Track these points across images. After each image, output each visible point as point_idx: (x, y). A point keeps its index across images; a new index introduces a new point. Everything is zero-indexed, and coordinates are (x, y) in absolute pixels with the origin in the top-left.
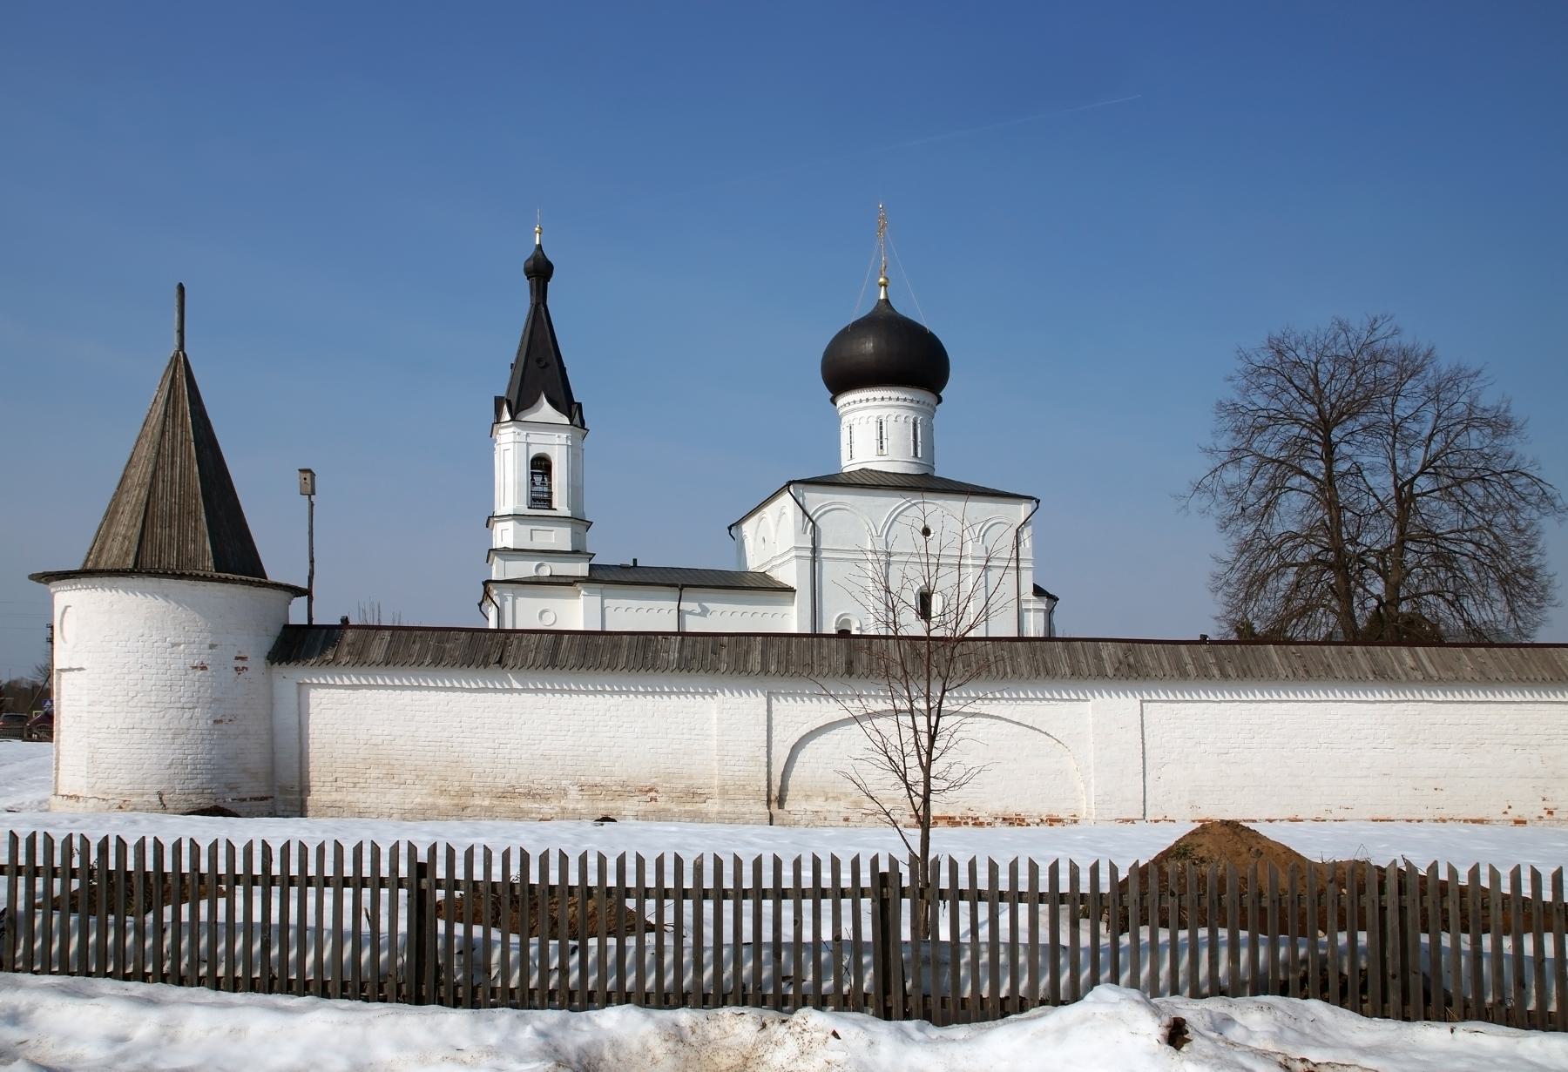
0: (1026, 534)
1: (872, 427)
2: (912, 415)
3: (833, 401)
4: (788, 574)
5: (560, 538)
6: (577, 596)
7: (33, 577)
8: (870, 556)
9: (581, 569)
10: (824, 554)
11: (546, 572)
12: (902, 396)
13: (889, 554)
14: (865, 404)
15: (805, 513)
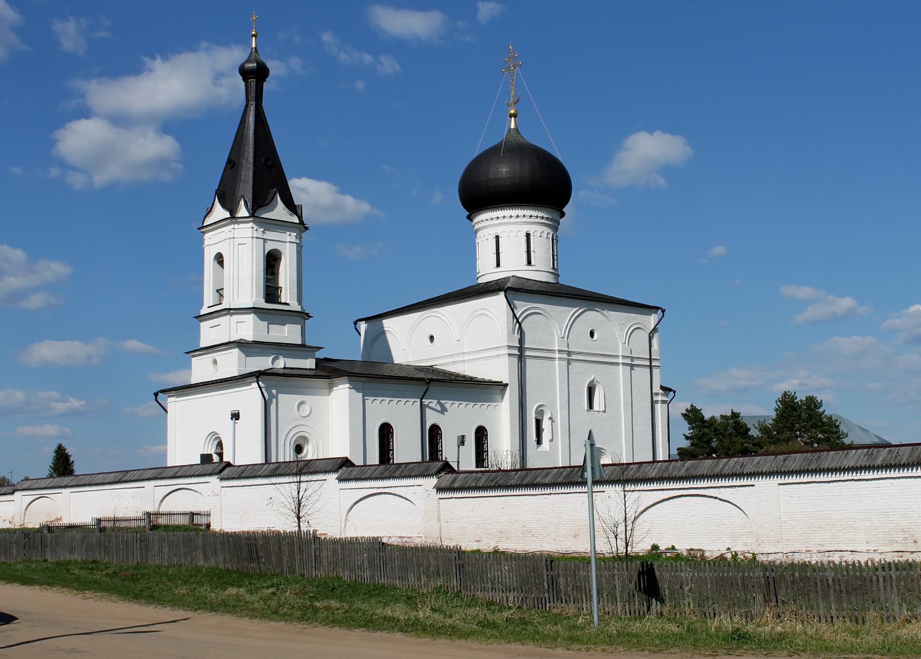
0: (655, 341)
1: (509, 240)
2: (547, 230)
3: (470, 218)
4: (498, 368)
5: (289, 333)
6: (331, 388)
7: (590, 432)
8: (557, 355)
9: (309, 363)
10: (527, 353)
11: (281, 363)
12: (540, 214)
13: (569, 353)
14: (495, 222)
15: (514, 315)
